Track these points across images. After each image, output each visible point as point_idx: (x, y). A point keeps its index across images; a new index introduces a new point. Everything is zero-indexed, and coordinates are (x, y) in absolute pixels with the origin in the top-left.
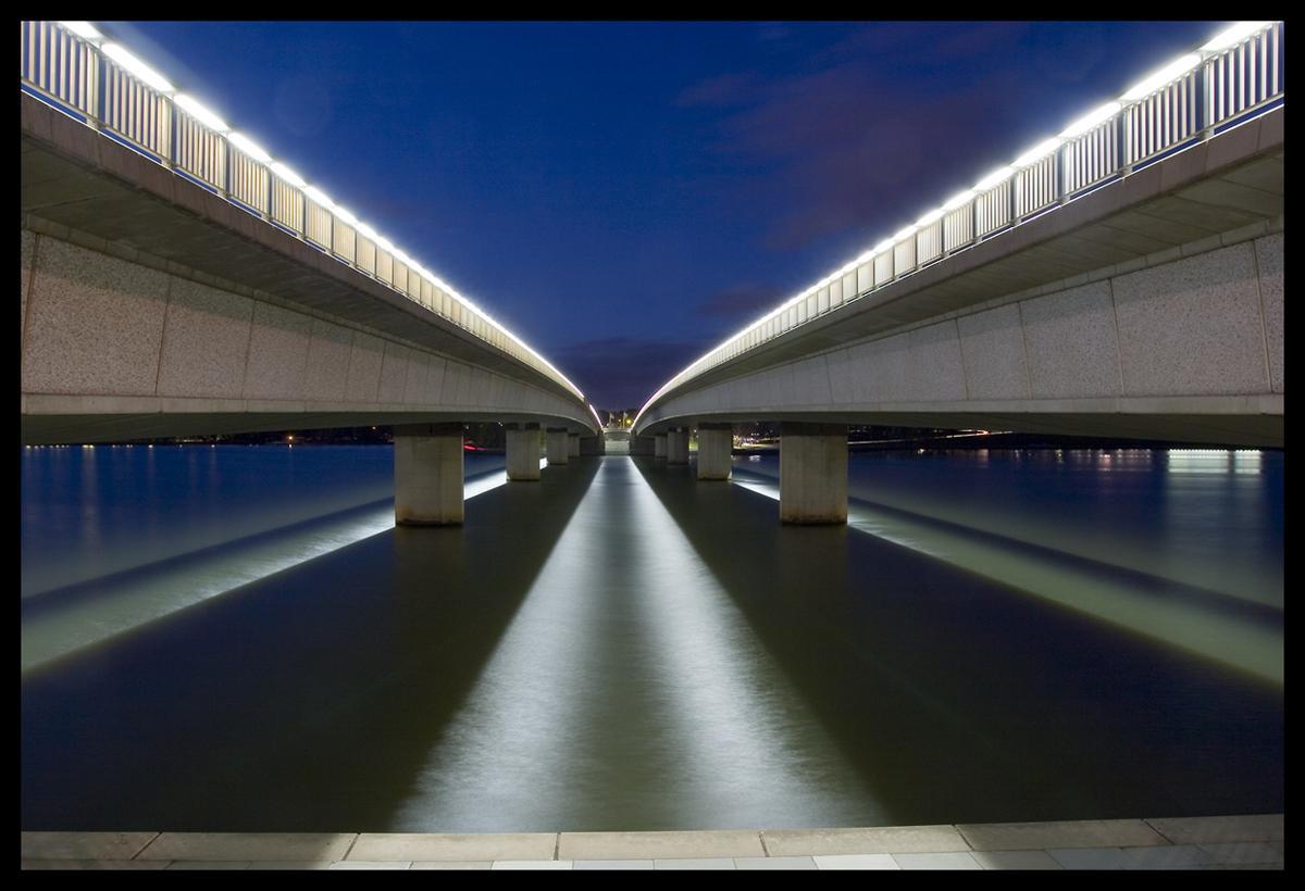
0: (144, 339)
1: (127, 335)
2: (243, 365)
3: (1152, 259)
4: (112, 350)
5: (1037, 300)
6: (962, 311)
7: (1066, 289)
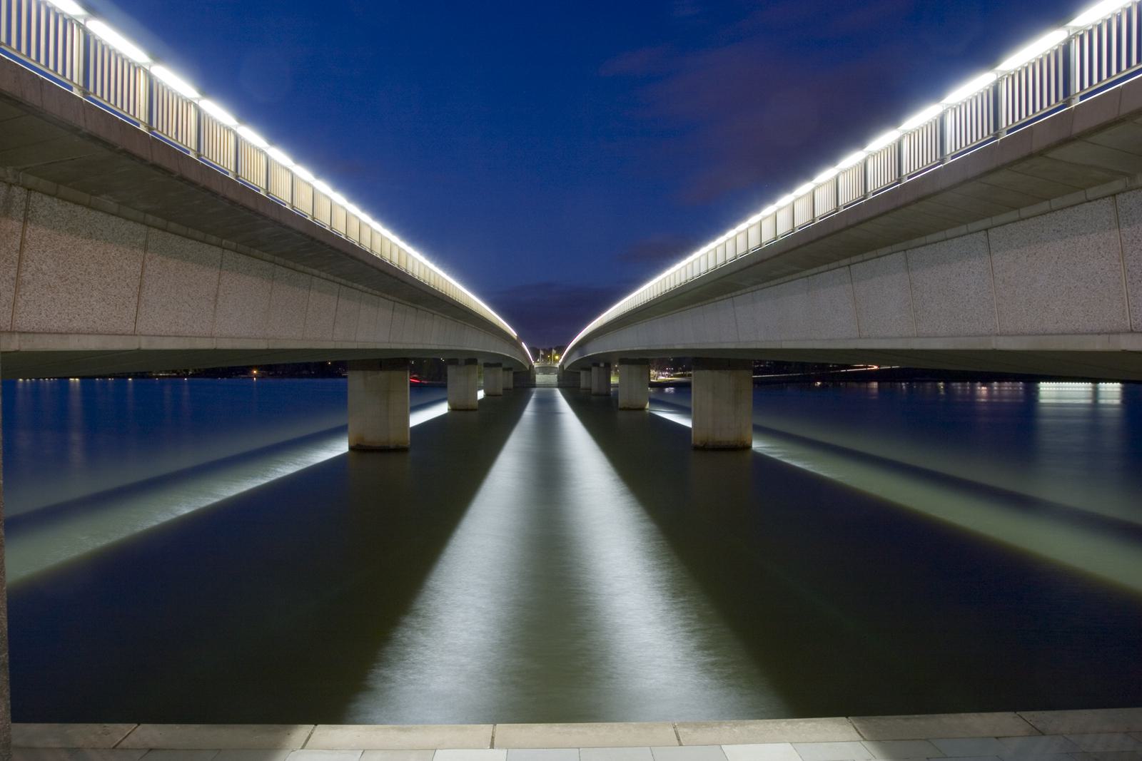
0: (124, 284)
1: (109, 280)
2: (212, 307)
3: (1025, 212)
4: (95, 293)
5: (922, 249)
6: (854, 259)
7: (947, 239)
